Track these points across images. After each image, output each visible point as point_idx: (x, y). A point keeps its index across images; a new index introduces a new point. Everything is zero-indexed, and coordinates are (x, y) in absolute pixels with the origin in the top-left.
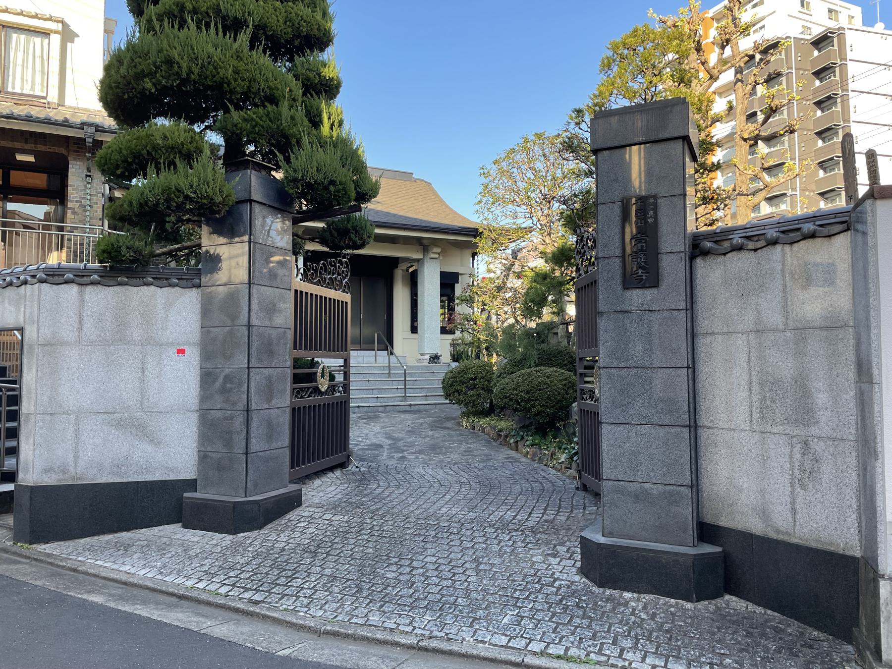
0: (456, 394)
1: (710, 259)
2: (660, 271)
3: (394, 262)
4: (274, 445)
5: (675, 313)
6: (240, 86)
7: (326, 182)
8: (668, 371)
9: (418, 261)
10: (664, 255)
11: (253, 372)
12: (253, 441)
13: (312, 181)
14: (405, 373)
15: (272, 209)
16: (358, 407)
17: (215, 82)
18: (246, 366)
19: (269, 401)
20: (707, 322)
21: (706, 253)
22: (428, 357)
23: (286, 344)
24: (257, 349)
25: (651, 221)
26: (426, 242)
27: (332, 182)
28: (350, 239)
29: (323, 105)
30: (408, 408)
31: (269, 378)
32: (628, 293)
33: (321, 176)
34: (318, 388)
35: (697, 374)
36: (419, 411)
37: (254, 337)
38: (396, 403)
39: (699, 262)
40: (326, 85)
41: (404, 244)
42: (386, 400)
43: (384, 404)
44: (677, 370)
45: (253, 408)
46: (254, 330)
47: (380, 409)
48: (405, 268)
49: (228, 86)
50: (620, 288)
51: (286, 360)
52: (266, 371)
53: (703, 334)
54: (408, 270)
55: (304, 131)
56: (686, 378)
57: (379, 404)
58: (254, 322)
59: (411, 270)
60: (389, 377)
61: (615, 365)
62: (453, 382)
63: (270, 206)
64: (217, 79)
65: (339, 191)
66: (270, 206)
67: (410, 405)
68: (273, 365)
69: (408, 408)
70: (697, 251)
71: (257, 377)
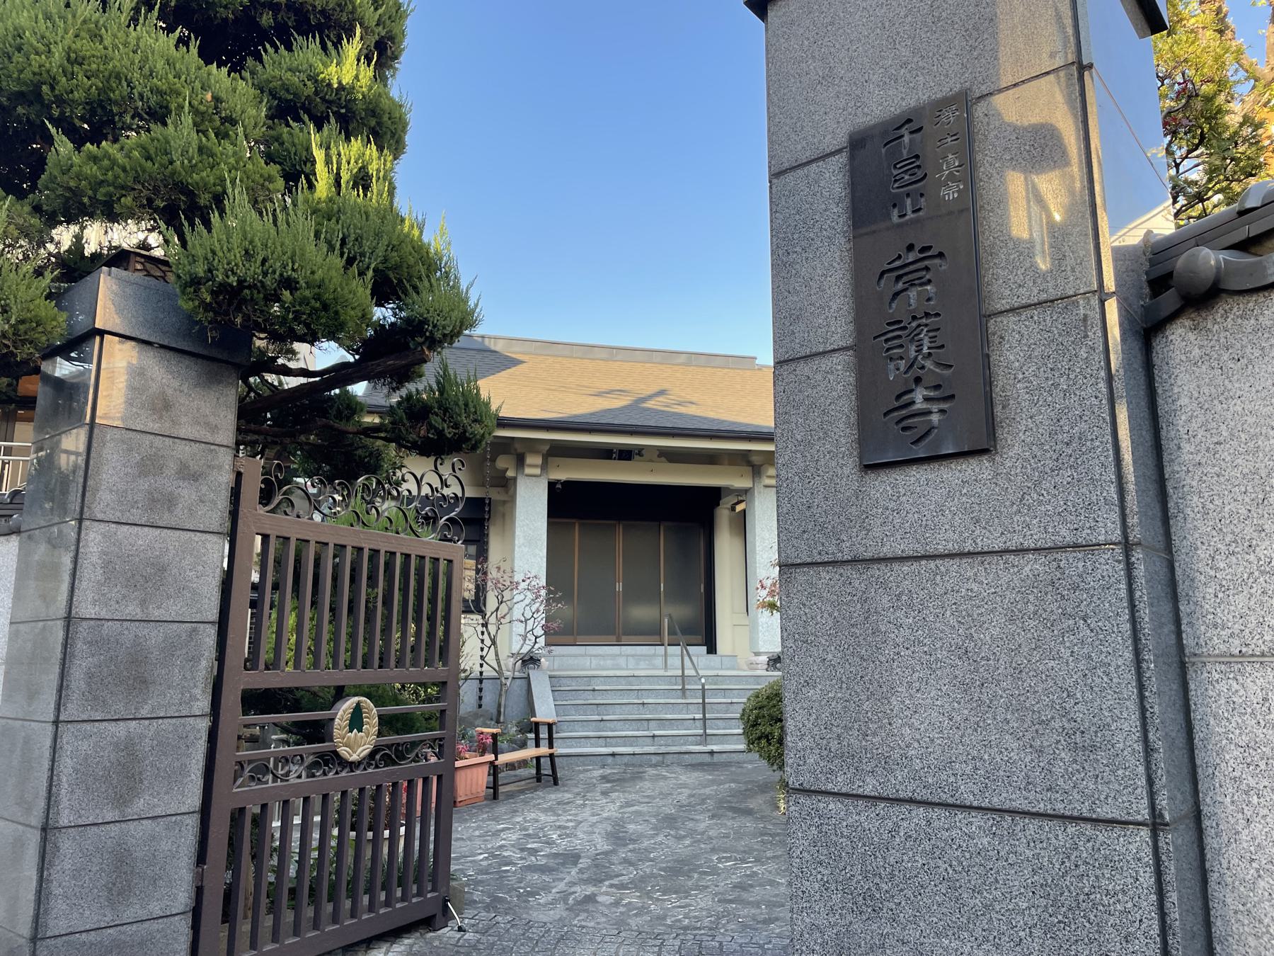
0: (763, 741)
1: (1228, 320)
2: (1000, 382)
3: (713, 496)
4: (129, 914)
5: (1074, 564)
6: (82, 88)
7: (268, 281)
8: (1063, 835)
9: (746, 491)
10: (1010, 321)
11: (68, 735)
12: (58, 906)
13: (233, 280)
14: (703, 690)
15: (169, 354)
16: (613, 755)
17: (25, 83)
18: (52, 718)
19: (121, 801)
20: (1240, 601)
21: (1203, 297)
22: (764, 659)
23: (195, 660)
24: (90, 676)
25: (950, 193)
26: (755, 459)
27: (290, 284)
28: (431, 426)
29: (315, 139)
30: (707, 758)
31: (128, 747)
32: (883, 485)
33: (255, 268)
34: (336, 753)
35: (1211, 842)
36: (727, 764)
37: (80, 645)
38: (684, 749)
39: (1180, 341)
40: (337, 102)
41: (730, 464)
42: (670, 741)
43: (663, 750)
44: (1102, 835)
45: (64, 821)
46: (83, 630)
47: (654, 759)
48: (729, 506)
49: (52, 88)
50: (849, 466)
51: (194, 698)
52: (120, 730)
53: (1229, 659)
54: (733, 509)
55: (233, 182)
56: (1147, 879)
57: (652, 749)
58: (86, 608)
59: (739, 508)
60: (684, 696)
61: (840, 783)
62: (757, 717)
63: (162, 346)
64: (27, 75)
65: (304, 302)
66: (162, 346)
67: (712, 753)
68: (144, 712)
69: (707, 758)
70: (1169, 300)
71: (85, 746)
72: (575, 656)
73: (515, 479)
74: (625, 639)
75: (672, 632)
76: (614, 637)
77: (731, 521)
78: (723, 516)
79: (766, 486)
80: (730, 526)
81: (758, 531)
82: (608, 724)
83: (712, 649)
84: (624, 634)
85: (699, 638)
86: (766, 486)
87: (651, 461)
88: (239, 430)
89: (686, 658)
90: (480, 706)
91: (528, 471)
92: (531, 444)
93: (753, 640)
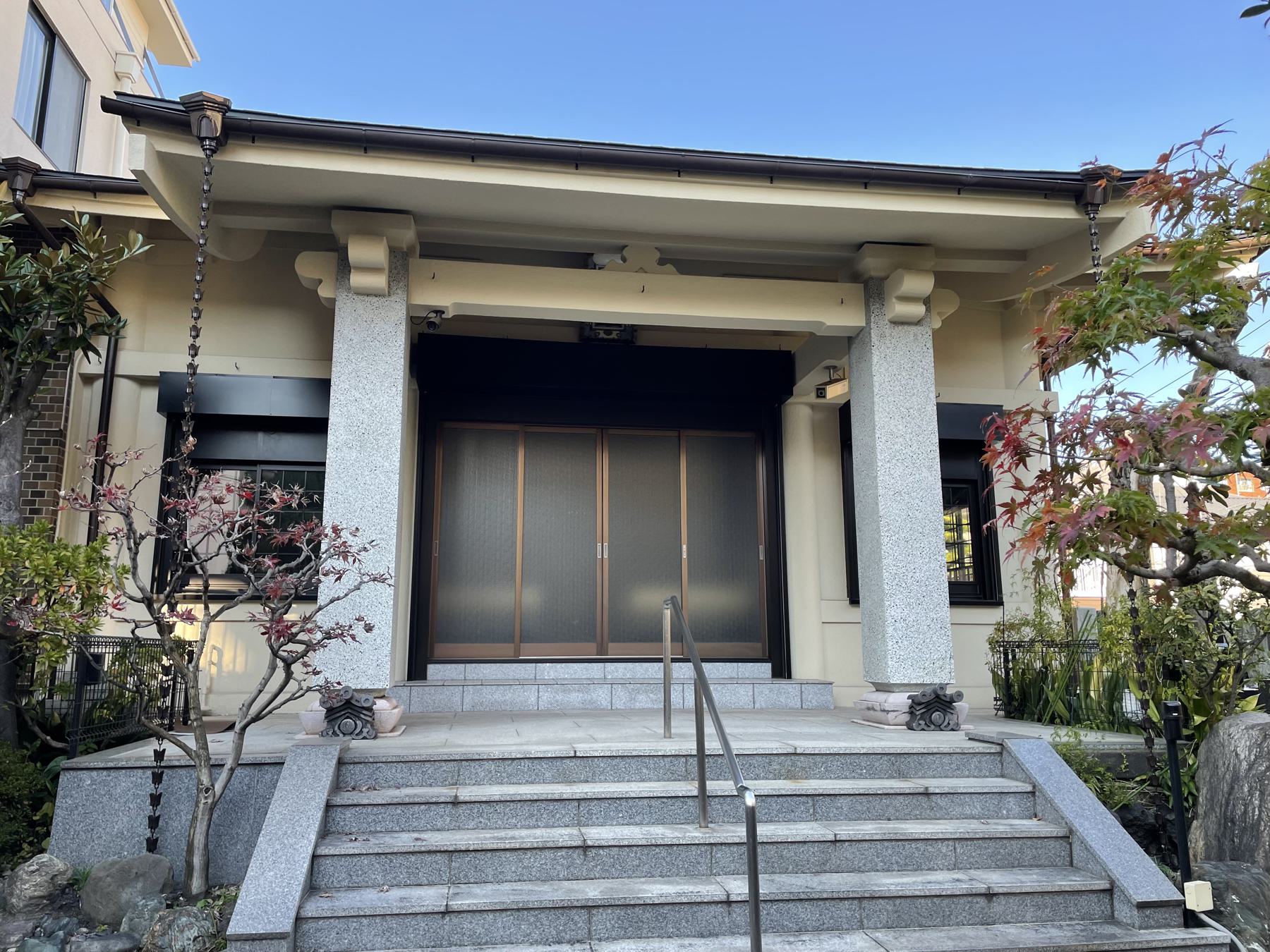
22: (900, 700)
54: (821, 393)
59: (835, 392)
72: (499, 684)
73: (333, 301)
74: (614, 649)
75: (677, 637)
76: (593, 646)
77: (815, 429)
78: (800, 416)
79: (898, 322)
80: (815, 451)
81: (880, 418)
82: (466, 923)
83: (782, 669)
84: (615, 639)
85: (757, 648)
86: (898, 322)
87: (642, 270)
88: (1039, 720)
89: (709, 729)
90: (152, 845)
91: (356, 279)
92: (368, 212)
93: (872, 652)
